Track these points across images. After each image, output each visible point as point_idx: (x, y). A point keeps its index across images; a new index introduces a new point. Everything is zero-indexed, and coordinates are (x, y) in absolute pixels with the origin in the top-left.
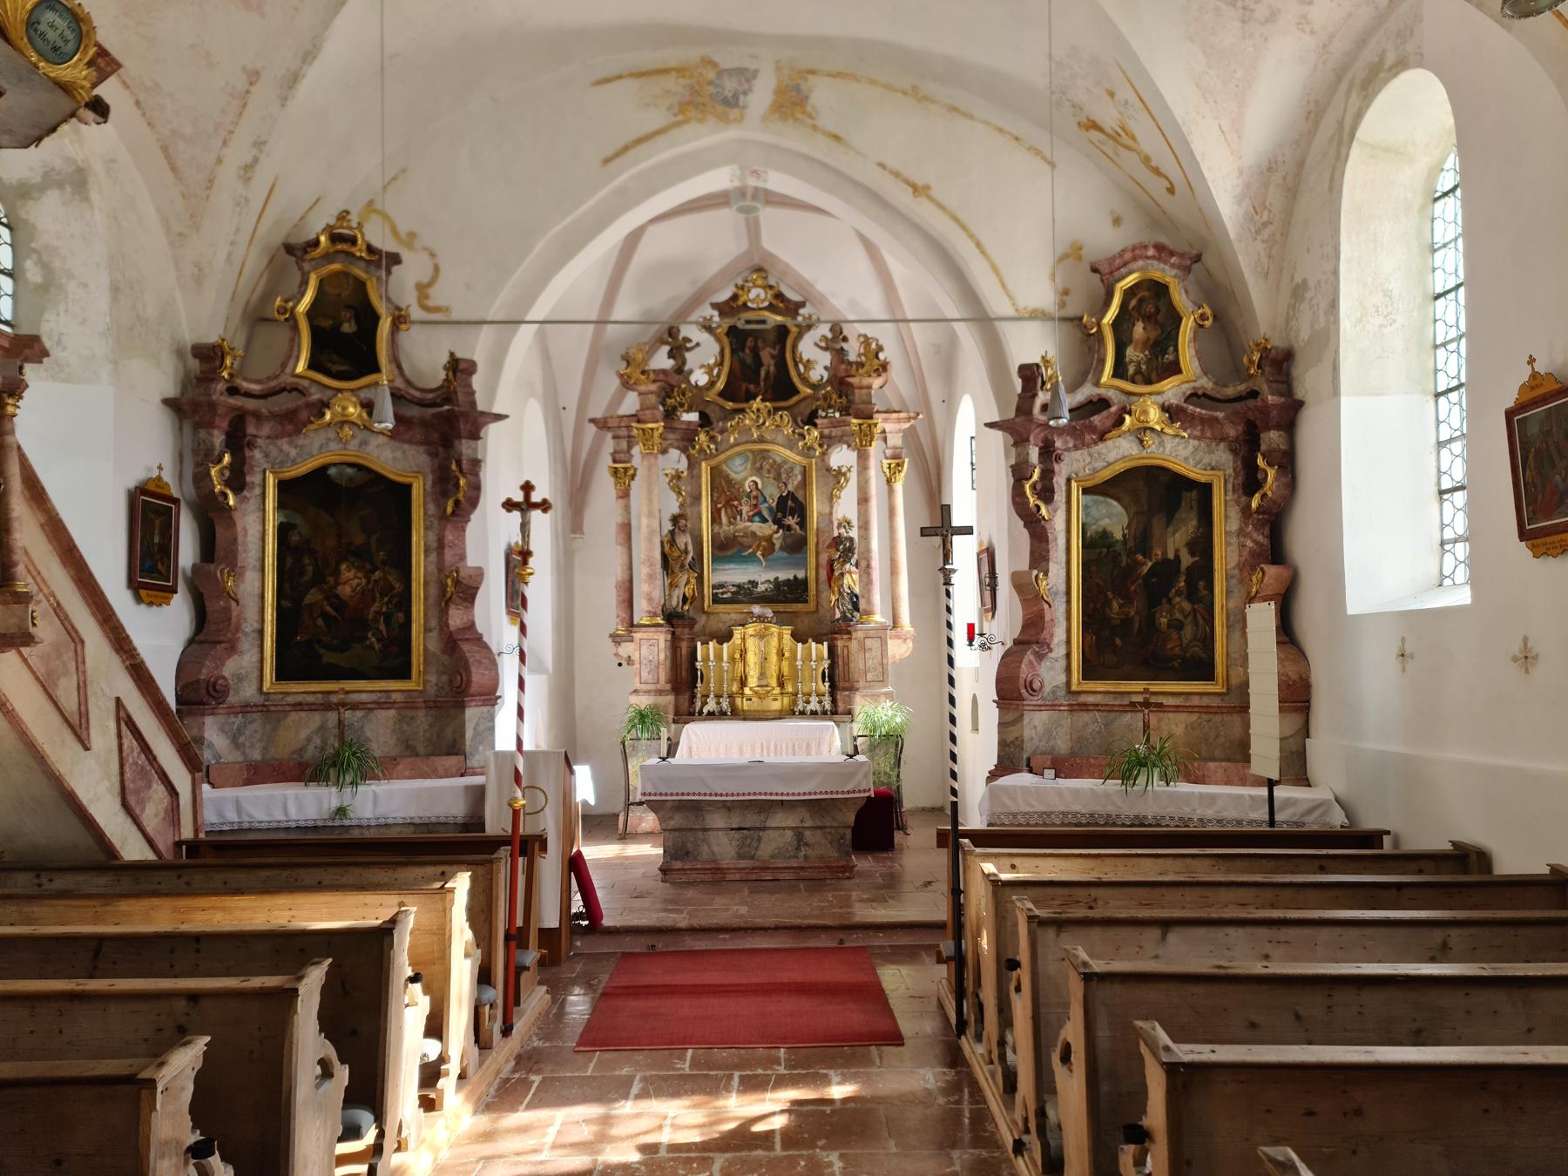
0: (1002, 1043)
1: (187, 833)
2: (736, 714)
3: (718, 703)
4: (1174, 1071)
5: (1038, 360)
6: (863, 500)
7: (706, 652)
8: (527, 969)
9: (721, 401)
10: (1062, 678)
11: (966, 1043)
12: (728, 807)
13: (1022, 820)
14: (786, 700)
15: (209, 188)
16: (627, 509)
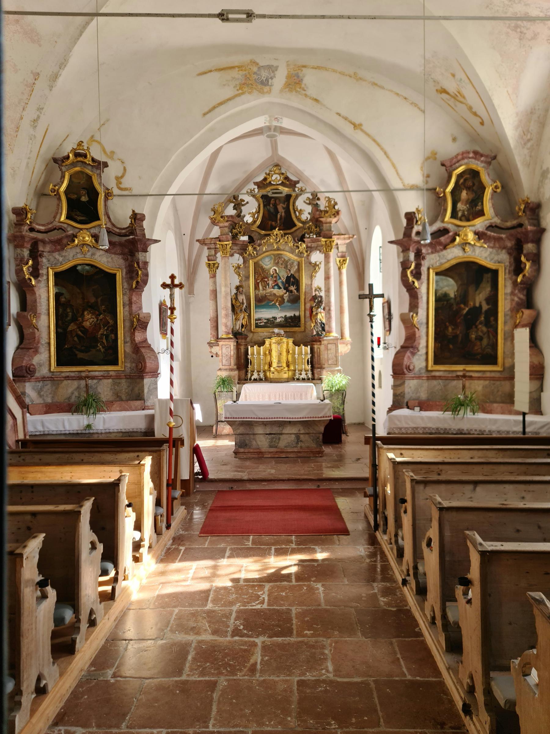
0: (396, 535)
1: (21, 436)
2: (267, 380)
3: (259, 375)
4: (483, 554)
5: (414, 210)
6: (327, 278)
7: (253, 351)
8: (176, 499)
9: (259, 230)
10: (424, 364)
11: (379, 535)
12: (265, 424)
13: (404, 431)
14: (290, 373)
15: (17, 131)
16: (215, 283)
